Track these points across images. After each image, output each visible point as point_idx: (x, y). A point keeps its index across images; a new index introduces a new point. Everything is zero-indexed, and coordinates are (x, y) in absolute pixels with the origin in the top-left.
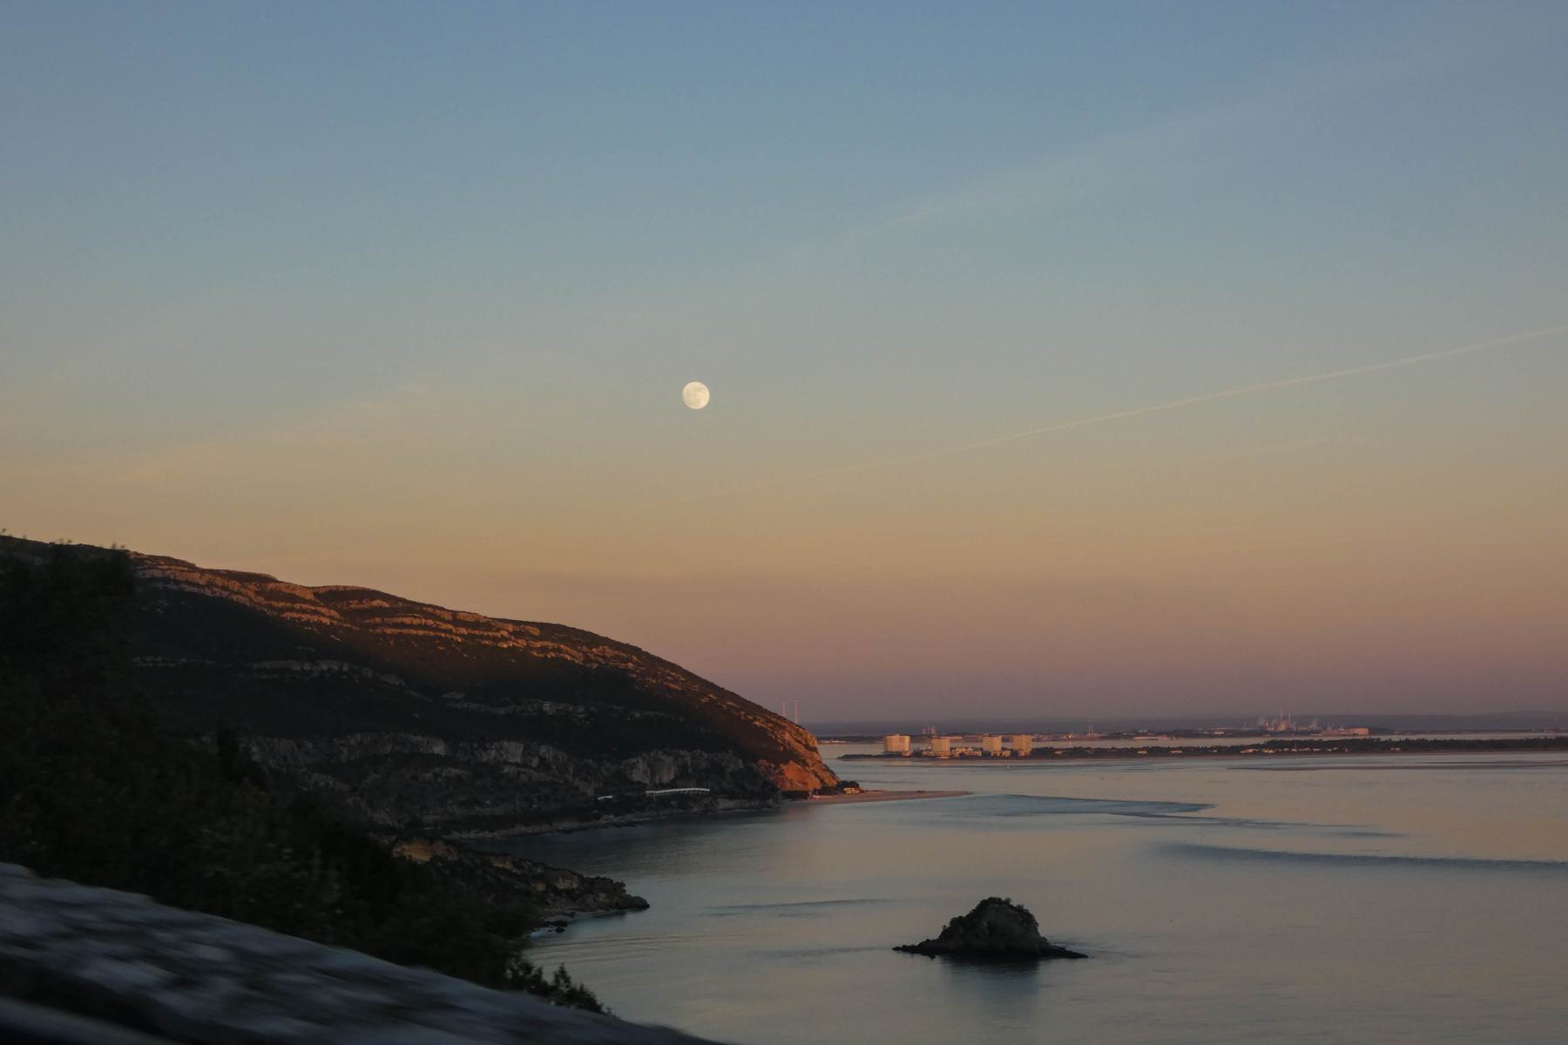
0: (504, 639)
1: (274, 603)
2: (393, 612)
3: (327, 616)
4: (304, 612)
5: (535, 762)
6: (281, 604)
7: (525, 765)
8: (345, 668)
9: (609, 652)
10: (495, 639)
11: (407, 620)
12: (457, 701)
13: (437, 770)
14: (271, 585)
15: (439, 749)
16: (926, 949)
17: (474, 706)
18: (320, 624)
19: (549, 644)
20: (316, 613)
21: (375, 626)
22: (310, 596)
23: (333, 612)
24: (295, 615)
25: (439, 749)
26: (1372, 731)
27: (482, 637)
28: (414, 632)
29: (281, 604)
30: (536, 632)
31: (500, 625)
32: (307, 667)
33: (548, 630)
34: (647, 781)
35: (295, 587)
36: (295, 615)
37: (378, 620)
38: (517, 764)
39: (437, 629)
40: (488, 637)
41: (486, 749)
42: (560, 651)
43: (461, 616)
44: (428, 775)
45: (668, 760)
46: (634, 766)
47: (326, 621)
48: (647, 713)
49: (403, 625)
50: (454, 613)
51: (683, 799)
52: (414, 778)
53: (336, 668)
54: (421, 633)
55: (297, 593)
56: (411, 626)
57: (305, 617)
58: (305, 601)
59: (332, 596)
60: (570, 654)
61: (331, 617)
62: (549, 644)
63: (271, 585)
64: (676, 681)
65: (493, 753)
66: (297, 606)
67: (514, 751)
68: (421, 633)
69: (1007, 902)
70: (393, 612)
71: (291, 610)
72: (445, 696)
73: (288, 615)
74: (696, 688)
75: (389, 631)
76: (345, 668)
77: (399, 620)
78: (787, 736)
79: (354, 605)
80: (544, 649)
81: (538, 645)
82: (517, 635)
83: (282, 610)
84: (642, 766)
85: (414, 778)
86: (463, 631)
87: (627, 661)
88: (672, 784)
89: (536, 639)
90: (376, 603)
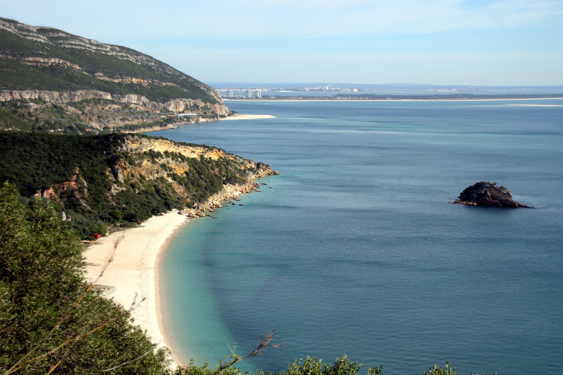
0: (108, 51)
1: (21, 33)
2: (66, 39)
3: (43, 39)
4: (34, 37)
5: (141, 103)
6: (25, 33)
7: (138, 104)
8: (61, 62)
9: (145, 59)
10: (105, 51)
11: (73, 42)
12: (101, 77)
13: (110, 106)
14: (19, 25)
15: (109, 97)
16: (455, 202)
17: (107, 79)
18: (40, 42)
19: (123, 54)
20: (38, 37)
21: (61, 44)
22: (35, 31)
23: (45, 38)
24: (31, 38)
25: (109, 97)
26: (359, 90)
27: (101, 50)
28: (77, 47)
29: (25, 33)
30: (118, 49)
31: (106, 46)
32: (46, 60)
33: (122, 48)
34: (174, 111)
35: (29, 26)
36: (31, 38)
37: (62, 41)
38: (135, 104)
39: (85, 47)
40: (103, 51)
41: (124, 97)
42: (127, 57)
43: (92, 42)
44: (107, 108)
45: (182, 103)
46: (170, 105)
47: (42, 41)
48: (168, 84)
49: (72, 44)
50: (89, 40)
51: (188, 118)
52: (103, 109)
53: (57, 61)
54: (79, 48)
55: (30, 29)
56: (75, 45)
57: (35, 39)
58: (84, 42)
59: (42, 31)
60: (132, 59)
61: (44, 39)
62: (123, 54)
63: (19, 25)
64: (170, 71)
65: (126, 99)
66: (31, 34)
67: (134, 98)
68: (79, 48)
69: (470, 187)
70: (66, 39)
71: (28, 35)
72: (96, 74)
73: (28, 38)
74: (178, 74)
75: (67, 46)
76: (61, 62)
77: (70, 42)
78: (212, 93)
79: (51, 35)
80: (122, 56)
81: (120, 54)
82: (112, 50)
83: (25, 35)
84: (173, 105)
85: (103, 109)
86: (94, 48)
87: (150, 62)
88: (183, 112)
89: (119, 52)
90: (60, 34)
